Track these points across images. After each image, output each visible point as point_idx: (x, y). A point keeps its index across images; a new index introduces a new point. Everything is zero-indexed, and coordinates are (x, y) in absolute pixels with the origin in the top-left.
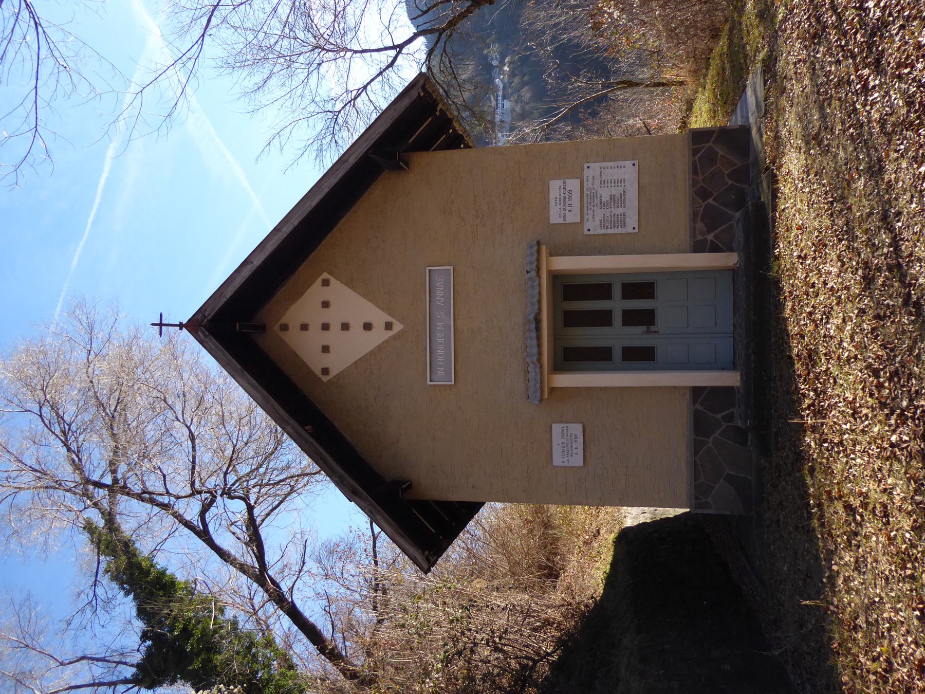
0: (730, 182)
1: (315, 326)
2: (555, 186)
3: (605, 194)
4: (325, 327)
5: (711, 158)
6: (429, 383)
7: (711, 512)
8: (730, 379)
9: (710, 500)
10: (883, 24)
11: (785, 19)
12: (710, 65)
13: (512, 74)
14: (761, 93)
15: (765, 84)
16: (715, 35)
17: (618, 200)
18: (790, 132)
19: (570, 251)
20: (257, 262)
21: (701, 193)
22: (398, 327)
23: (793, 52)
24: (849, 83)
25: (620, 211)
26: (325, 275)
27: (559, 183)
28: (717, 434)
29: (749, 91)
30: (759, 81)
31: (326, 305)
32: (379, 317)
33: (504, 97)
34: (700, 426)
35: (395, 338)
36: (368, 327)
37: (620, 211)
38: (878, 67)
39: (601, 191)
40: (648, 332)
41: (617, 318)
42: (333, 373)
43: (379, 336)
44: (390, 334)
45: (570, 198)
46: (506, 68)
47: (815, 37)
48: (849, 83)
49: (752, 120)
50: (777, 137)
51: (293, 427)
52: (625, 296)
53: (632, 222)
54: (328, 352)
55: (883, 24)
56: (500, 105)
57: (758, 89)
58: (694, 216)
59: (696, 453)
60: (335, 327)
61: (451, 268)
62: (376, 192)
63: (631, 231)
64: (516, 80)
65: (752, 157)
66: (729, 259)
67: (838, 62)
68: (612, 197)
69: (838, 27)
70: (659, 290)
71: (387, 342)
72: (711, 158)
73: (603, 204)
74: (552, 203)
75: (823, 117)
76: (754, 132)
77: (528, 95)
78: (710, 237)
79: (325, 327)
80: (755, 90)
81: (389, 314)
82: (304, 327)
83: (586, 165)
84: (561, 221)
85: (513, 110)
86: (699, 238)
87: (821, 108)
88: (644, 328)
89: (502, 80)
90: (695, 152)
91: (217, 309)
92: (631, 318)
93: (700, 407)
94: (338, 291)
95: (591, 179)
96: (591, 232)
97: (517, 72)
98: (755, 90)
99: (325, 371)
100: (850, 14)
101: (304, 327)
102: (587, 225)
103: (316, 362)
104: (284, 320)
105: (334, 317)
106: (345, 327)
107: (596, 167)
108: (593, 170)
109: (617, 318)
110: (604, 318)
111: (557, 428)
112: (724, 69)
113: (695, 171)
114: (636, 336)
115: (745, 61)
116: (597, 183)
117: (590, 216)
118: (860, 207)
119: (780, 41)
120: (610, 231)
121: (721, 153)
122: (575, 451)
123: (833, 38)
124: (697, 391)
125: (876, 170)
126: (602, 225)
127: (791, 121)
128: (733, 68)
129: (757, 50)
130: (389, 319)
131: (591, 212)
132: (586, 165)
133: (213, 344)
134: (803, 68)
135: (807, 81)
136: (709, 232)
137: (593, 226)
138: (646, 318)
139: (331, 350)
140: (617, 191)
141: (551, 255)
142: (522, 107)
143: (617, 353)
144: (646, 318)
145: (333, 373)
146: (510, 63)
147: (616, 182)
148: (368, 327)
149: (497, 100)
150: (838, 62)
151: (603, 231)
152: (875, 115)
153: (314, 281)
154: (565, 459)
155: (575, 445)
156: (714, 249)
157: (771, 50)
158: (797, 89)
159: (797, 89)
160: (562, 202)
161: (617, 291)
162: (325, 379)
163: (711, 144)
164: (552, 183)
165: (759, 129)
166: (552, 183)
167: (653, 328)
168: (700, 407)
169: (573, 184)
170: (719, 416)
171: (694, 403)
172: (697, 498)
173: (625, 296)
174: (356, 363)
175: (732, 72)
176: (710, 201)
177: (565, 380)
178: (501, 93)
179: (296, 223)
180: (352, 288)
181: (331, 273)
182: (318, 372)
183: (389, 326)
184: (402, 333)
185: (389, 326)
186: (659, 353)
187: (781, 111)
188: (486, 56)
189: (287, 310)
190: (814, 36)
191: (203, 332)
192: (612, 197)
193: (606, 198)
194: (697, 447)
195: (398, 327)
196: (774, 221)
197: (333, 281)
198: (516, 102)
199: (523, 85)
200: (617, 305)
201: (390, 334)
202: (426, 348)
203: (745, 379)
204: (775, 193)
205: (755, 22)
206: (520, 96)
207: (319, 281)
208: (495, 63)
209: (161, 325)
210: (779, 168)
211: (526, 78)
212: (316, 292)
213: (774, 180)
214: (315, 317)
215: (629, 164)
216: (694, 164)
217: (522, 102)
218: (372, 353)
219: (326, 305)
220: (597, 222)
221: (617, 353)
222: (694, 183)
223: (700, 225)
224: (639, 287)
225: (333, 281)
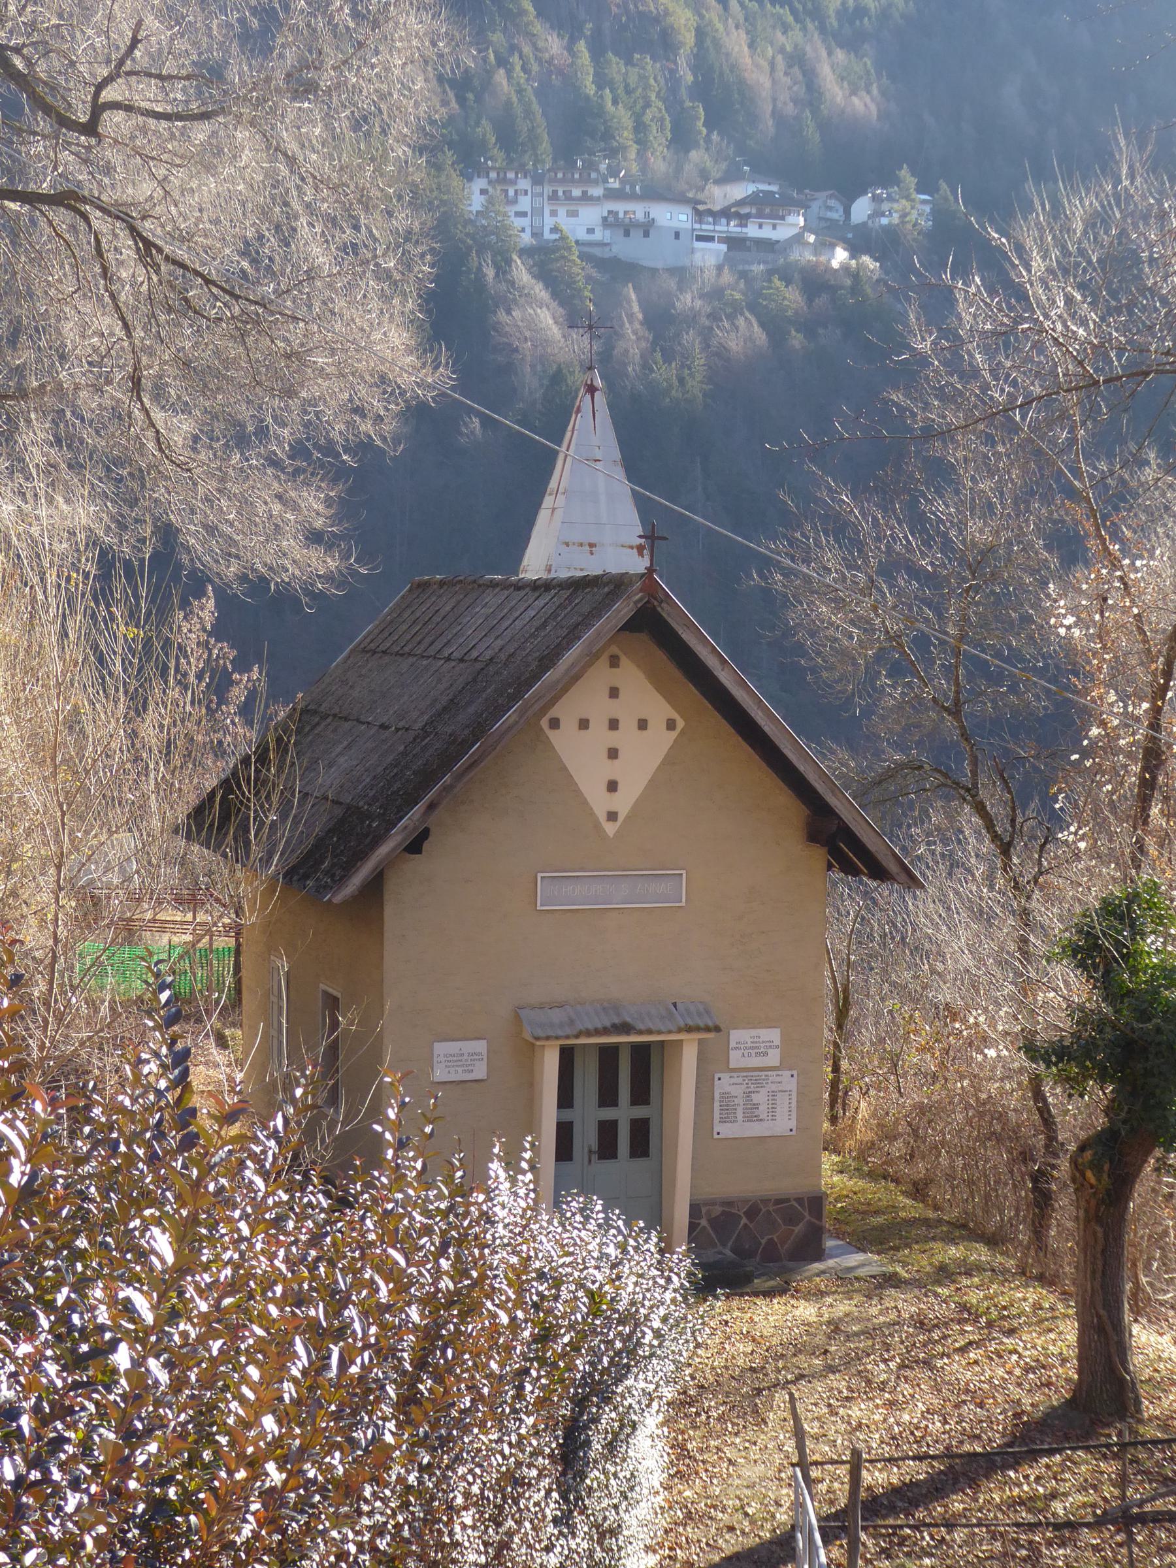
0: (763, 1241)
1: (614, 708)
2: (773, 1035)
3: (760, 1098)
4: (614, 724)
5: (792, 1218)
6: (540, 875)
10: (932, 1368)
11: (936, 1295)
12: (876, 1181)
13: (815, 283)
14: (862, 1272)
15: (874, 1277)
16: (918, 1191)
17: (752, 1115)
18: (831, 1306)
21: (753, 1211)
22: (610, 829)
23: (904, 1304)
24: (888, 1351)
25: (740, 1116)
26: (680, 724)
27: (777, 1042)
29: (859, 1257)
30: (875, 1270)
31: (643, 725)
32: (623, 802)
33: (735, 243)
35: (597, 826)
36: (612, 786)
37: (740, 1116)
38: (902, 1366)
39: (763, 1091)
40: (590, 1151)
41: (608, 1114)
42: (552, 735)
43: (600, 802)
44: (602, 817)
46: (840, 256)
47: (920, 1323)
48: (888, 1351)
49: (831, 1263)
50: (822, 1294)
51: (517, 722)
53: (725, 1130)
55: (932, 1368)
56: (707, 227)
57: (866, 1269)
58: (730, 1204)
61: (683, 904)
63: (716, 1130)
64: (792, 297)
65: (791, 1264)
67: (902, 1342)
68: (756, 1106)
69: (930, 1341)
70: (641, 1163)
71: (592, 814)
72: (792, 1218)
73: (748, 1095)
74: (754, 1032)
75: (856, 1334)
76: (817, 1266)
77: (735, 345)
78: (704, 1222)
79: (614, 724)
80: (863, 1265)
81: (628, 818)
82: (614, 693)
83: (795, 1073)
84: (732, 1044)
85: (682, 274)
86: (704, 1210)
87: (863, 1333)
88: (595, 1147)
89: (798, 239)
90: (799, 1200)
91: (669, 620)
92: (608, 1130)
94: (660, 741)
95: (778, 1079)
96: (717, 1082)
97: (822, 301)
98: (863, 1265)
99: (555, 724)
100: (939, 1348)
101: (614, 693)
103: (567, 710)
104: (625, 661)
106: (613, 754)
107: (792, 1085)
108: (789, 1082)
109: (608, 1114)
110: (608, 1097)
111: (481, 1046)
112: (877, 1212)
113: (778, 1201)
114: (586, 1137)
115: (891, 1248)
116: (774, 1087)
118: (803, 1361)
119: (917, 1292)
120: (717, 1105)
121: (797, 1229)
122: (452, 1070)
123: (921, 1337)
125: (832, 1369)
126: (725, 1095)
127: (843, 1307)
128: (881, 1228)
129: (905, 1264)
130: (621, 818)
131: (740, 1080)
132: (795, 1073)
134: (893, 1316)
135: (882, 1319)
136: (710, 1221)
137: (725, 1084)
138: (607, 1148)
140: (763, 1111)
141: (700, 1041)
142: (691, 319)
143: (568, 1115)
144: (607, 1148)
145: (552, 735)
146: (856, 276)
147: (772, 1110)
148: (612, 786)
149: (726, 213)
150: (902, 1342)
151: (717, 1096)
152: (869, 1367)
153: (674, 707)
154: (442, 1058)
156: (692, 1227)
157: (906, 1282)
158: (874, 1311)
159: (874, 1311)
160: (755, 1045)
161: (640, 1112)
162: (544, 723)
163: (808, 1217)
165: (823, 1272)
167: (595, 1157)
169: (774, 1058)
175: (874, 1228)
176: (744, 1220)
177: (551, 1063)
178: (752, 231)
179: (766, 729)
180: (663, 763)
181: (682, 732)
182: (553, 712)
183: (612, 816)
185: (612, 816)
186: (566, 1165)
187: (849, 1295)
188: (888, 179)
189: (638, 666)
190: (922, 1323)
191: (641, 600)
192: (756, 1106)
193: (756, 1098)
195: (610, 829)
196: (742, 1295)
197: (673, 735)
198: (716, 294)
199: (774, 325)
200: (624, 1113)
201: (602, 817)
204: (769, 1294)
205: (938, 1258)
206: (734, 311)
207: (675, 715)
208: (862, 209)
210: (793, 1296)
211: (797, 340)
213: (782, 1291)
214: (623, 709)
215: (793, 1124)
216: (788, 1200)
217: (714, 316)
219: (643, 725)
220: (728, 1089)
221: (568, 1115)
222: (765, 1201)
223: (718, 1210)
224: (642, 1139)
225: (673, 735)
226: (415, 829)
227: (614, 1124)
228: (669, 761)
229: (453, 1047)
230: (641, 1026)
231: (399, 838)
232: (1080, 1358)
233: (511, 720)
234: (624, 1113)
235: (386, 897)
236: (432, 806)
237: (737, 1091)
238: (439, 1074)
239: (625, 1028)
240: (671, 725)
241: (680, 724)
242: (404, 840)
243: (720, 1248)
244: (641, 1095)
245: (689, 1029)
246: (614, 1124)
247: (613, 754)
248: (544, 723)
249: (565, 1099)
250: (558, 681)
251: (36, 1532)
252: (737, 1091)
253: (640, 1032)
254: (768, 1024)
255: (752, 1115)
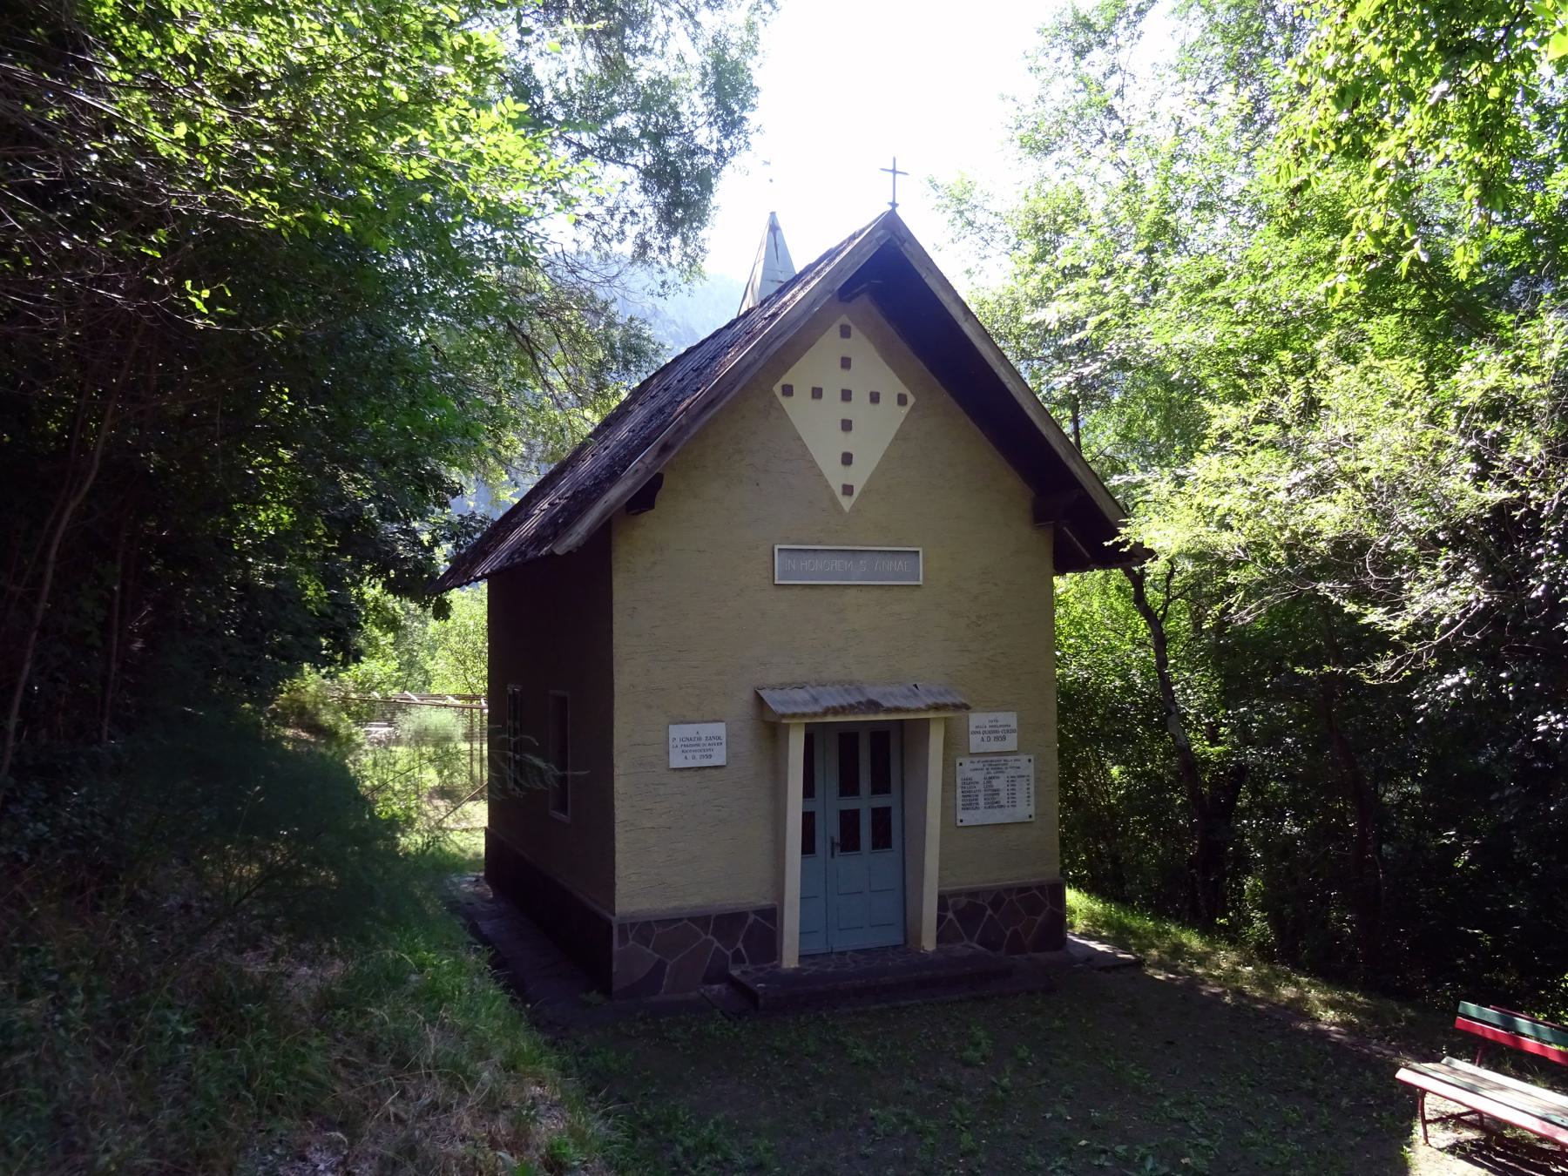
2: (1010, 719)
3: (1000, 783)
4: (846, 395)
7: (616, 946)
8: (790, 959)
9: (631, 942)
19: (948, 744)
20: (967, 328)
22: (847, 503)
25: (981, 802)
26: (911, 400)
27: (1014, 726)
28: (717, 944)
31: (875, 398)
32: (859, 475)
34: (727, 922)
35: (833, 498)
36: (847, 459)
37: (981, 802)
39: (1003, 777)
41: (850, 804)
42: (785, 402)
43: (836, 476)
44: (838, 491)
45: (997, 739)
51: (756, 361)
52: (875, 811)
53: (968, 818)
54: (844, 421)
58: (973, 894)
59: (693, 919)
60: (846, 410)
62: (1011, 481)
66: (929, 943)
68: (996, 792)
71: (828, 486)
74: (992, 716)
78: (950, 915)
79: (846, 395)
81: (864, 492)
84: (972, 729)
86: (950, 902)
88: (837, 839)
92: (849, 821)
93: (752, 917)
99: (788, 391)
102: (966, 761)
105: (858, 409)
106: (847, 426)
107: (1029, 770)
108: (1026, 766)
109: (850, 804)
110: (849, 786)
111: (720, 729)
114: (828, 829)
116: (1012, 772)
117: (976, 766)
120: (959, 791)
121: (1039, 919)
122: (689, 755)
124: (771, 916)
126: (968, 781)
133: (1016, 375)
136: (955, 913)
138: (849, 840)
139: (816, 401)
140: (1003, 797)
144: (849, 840)
145: (785, 402)
148: (847, 459)
155: (698, 755)
156: (940, 919)
161: (880, 801)
162: (777, 389)
164: (1014, 715)
166: (1014, 715)
168: (752, 917)
169: (1011, 743)
170: (740, 945)
171: (757, 912)
172: (633, 925)
173: (875, 811)
174: (800, 439)
176: (989, 912)
180: (896, 438)
181: (913, 408)
184: (840, 511)
185: (848, 490)
192: (996, 792)
193: (996, 784)
194: (702, 920)
195: (847, 503)
200: (865, 803)
202: (819, 543)
203: (794, 977)
207: (904, 390)
209: (894, 171)
212: (890, 384)
215: (1031, 810)
218: (812, 464)
219: (875, 398)
220: (970, 774)
222: (1009, 890)
223: (964, 901)
225: (905, 410)
226: (648, 471)
227: (856, 813)
228: (901, 437)
229: (689, 730)
230: (886, 704)
231: (630, 483)
232: (488, 832)
233: (750, 358)
234: (865, 803)
235: (615, 566)
236: (665, 448)
237: (978, 777)
238: (677, 761)
239: (874, 706)
240: (902, 400)
241: (911, 400)
242: (636, 484)
243: (966, 941)
244: (881, 784)
245: (937, 707)
246: (856, 813)
247: (847, 426)
248: (777, 389)
249: (809, 791)
250: (798, 320)
251: (1502, 61)
252: (978, 777)
253: (888, 710)
254: (1004, 707)
255: (993, 803)
